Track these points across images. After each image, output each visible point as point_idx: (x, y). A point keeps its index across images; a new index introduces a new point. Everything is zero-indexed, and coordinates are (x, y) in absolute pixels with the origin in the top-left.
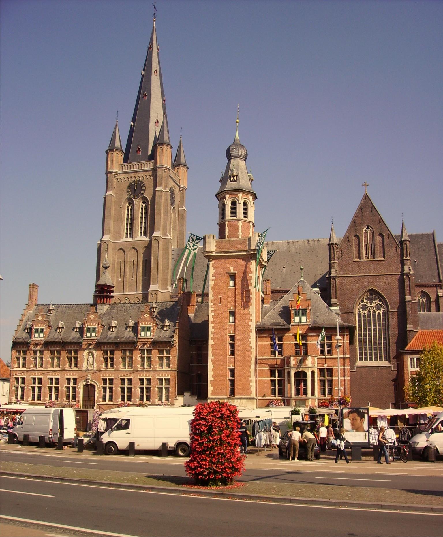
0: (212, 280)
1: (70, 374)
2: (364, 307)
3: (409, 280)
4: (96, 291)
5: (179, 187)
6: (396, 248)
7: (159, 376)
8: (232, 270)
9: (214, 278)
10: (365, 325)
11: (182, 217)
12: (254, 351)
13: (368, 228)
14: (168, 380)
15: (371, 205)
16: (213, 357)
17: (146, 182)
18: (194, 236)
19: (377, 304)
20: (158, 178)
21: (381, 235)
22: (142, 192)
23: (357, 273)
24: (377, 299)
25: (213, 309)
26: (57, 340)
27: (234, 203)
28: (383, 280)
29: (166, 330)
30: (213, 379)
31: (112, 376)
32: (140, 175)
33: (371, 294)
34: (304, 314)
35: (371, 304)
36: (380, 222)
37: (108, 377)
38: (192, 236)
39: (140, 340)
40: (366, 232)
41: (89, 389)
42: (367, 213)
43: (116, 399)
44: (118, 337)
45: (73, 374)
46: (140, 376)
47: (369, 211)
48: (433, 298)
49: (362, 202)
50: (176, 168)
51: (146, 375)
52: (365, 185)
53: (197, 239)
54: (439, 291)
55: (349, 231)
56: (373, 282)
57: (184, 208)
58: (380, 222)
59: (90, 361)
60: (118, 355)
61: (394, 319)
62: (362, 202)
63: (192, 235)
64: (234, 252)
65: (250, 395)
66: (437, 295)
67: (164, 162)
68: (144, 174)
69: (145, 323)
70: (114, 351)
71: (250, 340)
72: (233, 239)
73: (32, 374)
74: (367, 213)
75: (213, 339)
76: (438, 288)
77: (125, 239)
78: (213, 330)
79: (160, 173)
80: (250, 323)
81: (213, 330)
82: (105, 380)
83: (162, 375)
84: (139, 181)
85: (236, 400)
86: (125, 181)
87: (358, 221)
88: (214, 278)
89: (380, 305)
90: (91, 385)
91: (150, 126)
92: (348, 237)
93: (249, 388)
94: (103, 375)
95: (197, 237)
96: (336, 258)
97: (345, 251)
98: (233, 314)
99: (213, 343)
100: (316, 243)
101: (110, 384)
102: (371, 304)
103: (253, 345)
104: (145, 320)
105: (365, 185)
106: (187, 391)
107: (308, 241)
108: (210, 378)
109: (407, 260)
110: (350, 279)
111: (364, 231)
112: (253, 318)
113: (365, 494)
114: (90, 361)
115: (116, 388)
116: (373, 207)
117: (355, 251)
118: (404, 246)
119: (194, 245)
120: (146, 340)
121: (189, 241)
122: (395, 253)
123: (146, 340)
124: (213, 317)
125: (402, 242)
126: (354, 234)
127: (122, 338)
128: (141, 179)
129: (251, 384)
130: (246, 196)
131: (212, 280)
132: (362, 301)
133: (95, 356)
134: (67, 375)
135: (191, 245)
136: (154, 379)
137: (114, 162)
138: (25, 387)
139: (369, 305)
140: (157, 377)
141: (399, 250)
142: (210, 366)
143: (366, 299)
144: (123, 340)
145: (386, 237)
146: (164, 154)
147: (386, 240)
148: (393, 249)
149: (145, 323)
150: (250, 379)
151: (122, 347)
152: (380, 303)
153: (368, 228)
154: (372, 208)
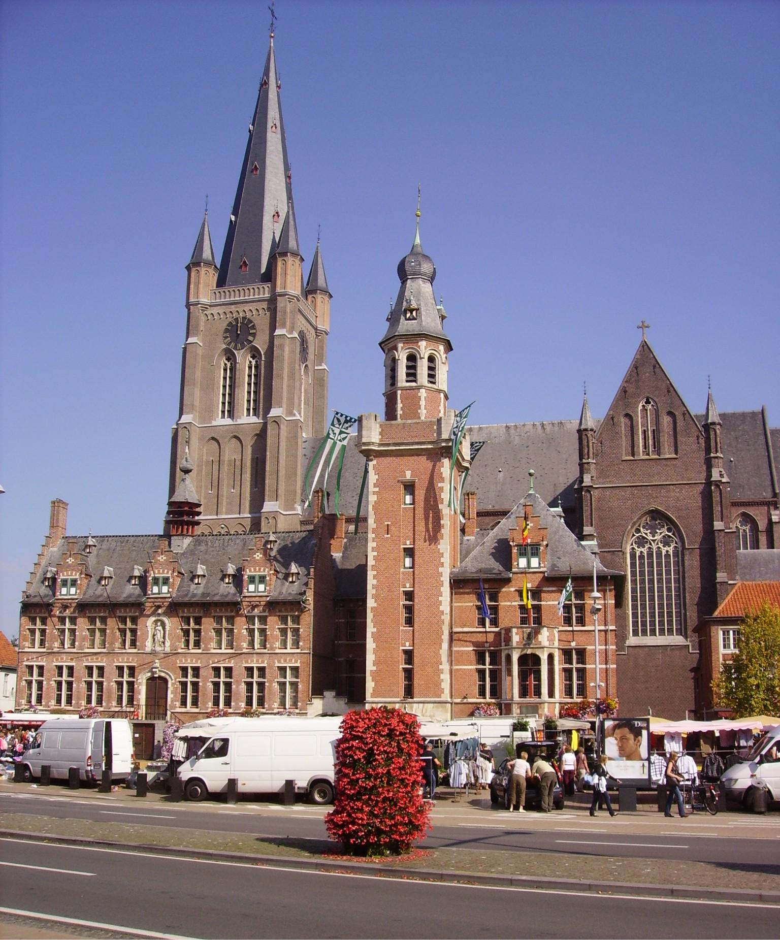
0: (374, 493)
1: (123, 659)
2: (642, 541)
3: (721, 494)
4: (169, 513)
5: (316, 329)
6: (698, 437)
7: (279, 662)
8: (408, 475)
9: (377, 489)
10: (642, 573)
11: (320, 382)
12: (446, 618)
13: (648, 402)
14: (295, 670)
15: (653, 361)
16: (375, 630)
17: (257, 321)
18: (342, 415)
19: (664, 536)
20: (278, 314)
21: (670, 413)
22: (250, 338)
23: (629, 481)
24: (663, 526)
25: (374, 544)
26: (100, 599)
27: (412, 358)
28: (675, 493)
29: (293, 582)
30: (375, 668)
31: (197, 662)
32: (247, 308)
33: (653, 519)
34: (535, 553)
35: (654, 536)
36: (669, 392)
37: (190, 664)
38: (338, 416)
39: (247, 599)
40: (644, 409)
41: (157, 685)
42: (646, 375)
43: (205, 703)
44: (208, 595)
45: (128, 659)
46: (247, 662)
47: (650, 373)
48: (762, 525)
49: (638, 356)
50: (310, 297)
51: (258, 661)
52: (643, 326)
53: (346, 422)
54: (772, 512)
55: (615, 406)
56: (657, 497)
57: (324, 366)
58: (669, 392)
59: (159, 636)
60: (208, 625)
61: (693, 562)
62: (638, 356)
63: (337, 413)
64: (412, 444)
65: (439, 696)
66: (770, 520)
67: (288, 284)
68: (253, 306)
69: (255, 569)
70: (200, 618)
71: (440, 598)
72: (409, 421)
73: (57, 660)
74: (646, 375)
75: (375, 597)
76: (772, 508)
77: (221, 421)
78: (375, 582)
79: (282, 305)
80: (441, 569)
81: (375, 582)
82: (184, 670)
83: (285, 661)
84: (244, 318)
85: (415, 705)
86: (221, 318)
87: (631, 389)
88: (377, 489)
89: (669, 537)
90: (160, 678)
91: (264, 222)
92: (612, 418)
93: (438, 684)
94: (181, 661)
95: (346, 417)
96: (591, 455)
97: (607, 443)
98: (410, 552)
99: (375, 605)
100: (556, 428)
101: (194, 676)
102: (654, 536)
103: (445, 607)
104: (256, 563)
105: (643, 326)
106: (329, 689)
107: (543, 425)
108: (370, 666)
109: (717, 457)
110: (617, 491)
111: (640, 407)
112: (446, 560)
113: (643, 870)
114: (159, 636)
115: (205, 684)
116: (656, 365)
117: (624, 442)
118: (712, 433)
119: (341, 432)
120: (257, 599)
121: (333, 424)
122: (695, 447)
123: (257, 599)
124: (375, 558)
125: (707, 427)
126: (624, 413)
127: (215, 595)
128: (248, 315)
129: (442, 676)
130: (433, 345)
131: (374, 493)
132: (638, 531)
133: (168, 628)
134: (118, 660)
135: (337, 431)
136: (271, 667)
137: (201, 286)
138: (44, 683)
139: (650, 537)
140: (277, 665)
141: (702, 441)
142: (370, 645)
143: (644, 527)
144: (217, 598)
145: (679, 418)
146: (289, 272)
147: (680, 423)
148: (693, 439)
149: (255, 569)
150: (441, 667)
151: (216, 611)
152: (670, 534)
153: (648, 402)
154: (654, 367)
